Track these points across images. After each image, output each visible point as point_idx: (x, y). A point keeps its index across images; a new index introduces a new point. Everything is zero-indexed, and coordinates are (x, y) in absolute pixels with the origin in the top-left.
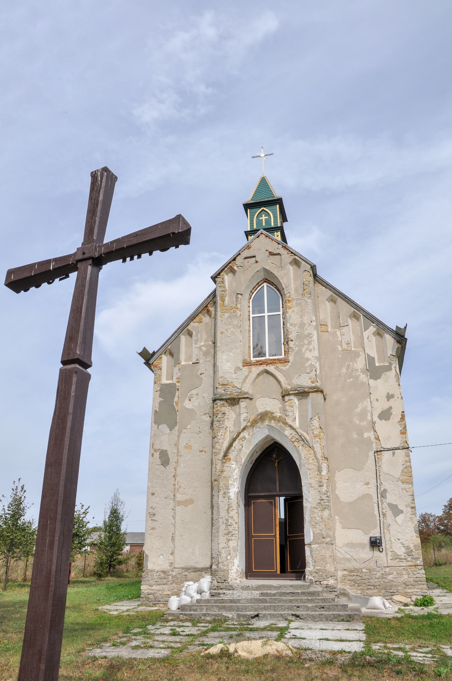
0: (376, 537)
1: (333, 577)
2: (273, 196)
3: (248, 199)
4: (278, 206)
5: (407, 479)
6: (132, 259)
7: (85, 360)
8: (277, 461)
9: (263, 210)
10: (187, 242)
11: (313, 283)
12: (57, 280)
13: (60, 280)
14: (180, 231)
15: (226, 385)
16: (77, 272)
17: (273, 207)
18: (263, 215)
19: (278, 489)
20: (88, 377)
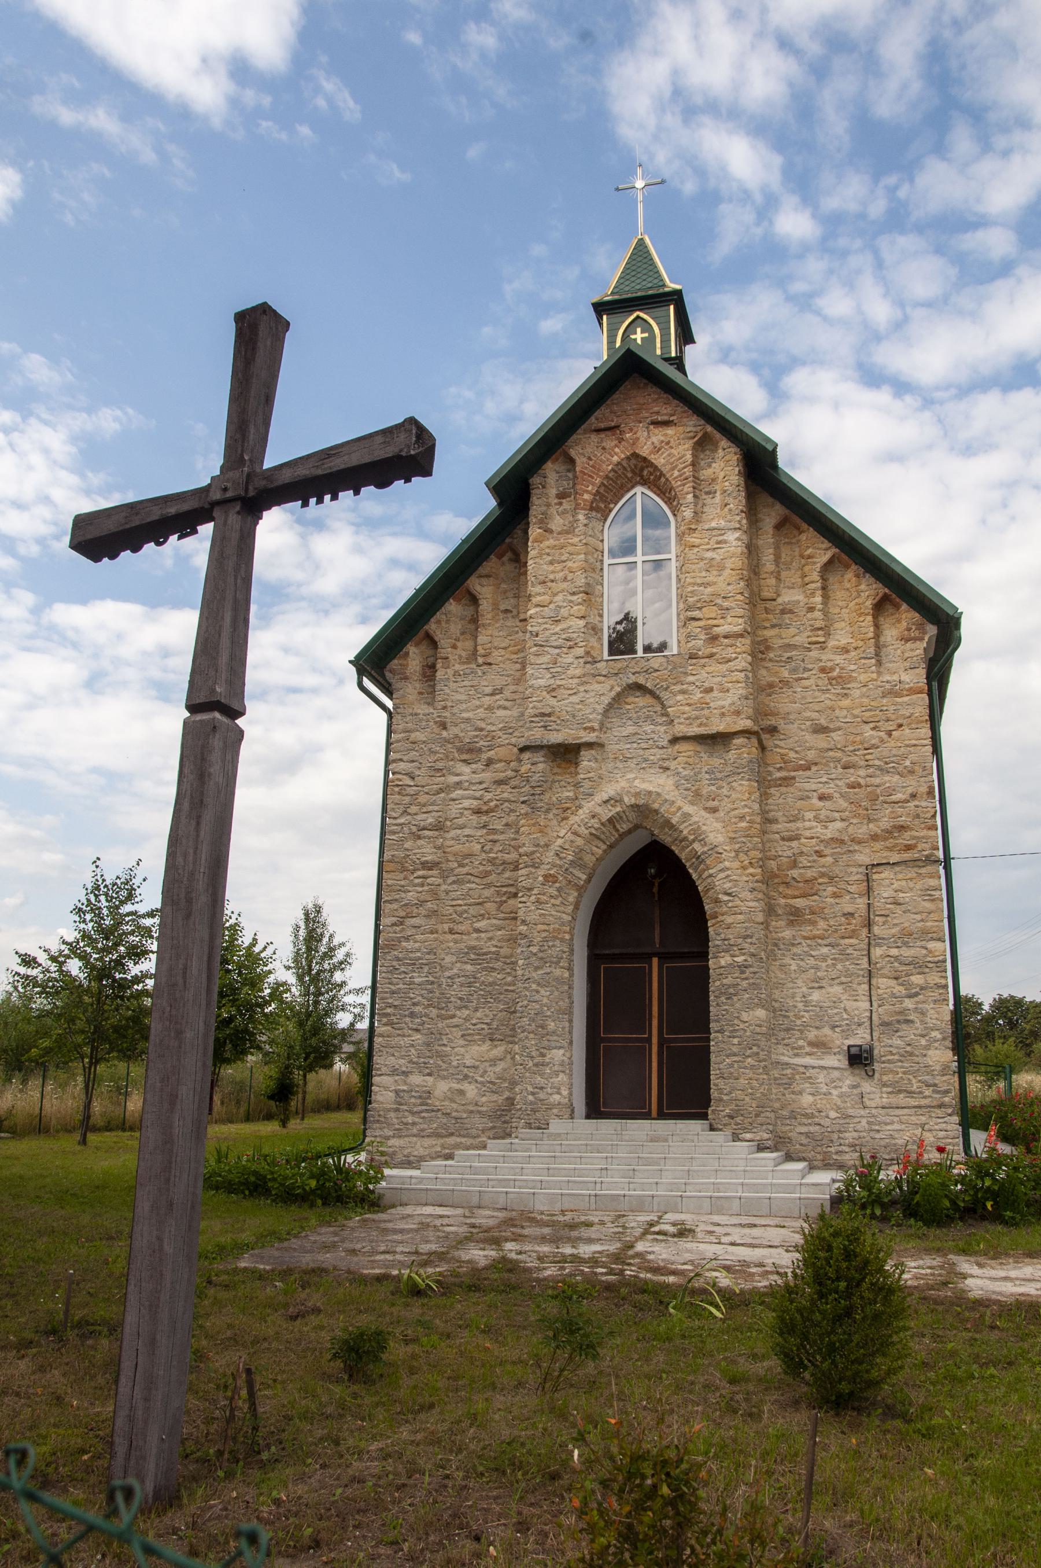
0: (860, 1046)
1: (764, 1127)
2: (661, 284)
3: (606, 292)
4: (672, 307)
5: (932, 927)
6: (320, 501)
7: (236, 706)
8: (657, 882)
9: (638, 317)
10: (427, 472)
11: (737, 502)
12: (173, 538)
13: (179, 538)
14: (412, 452)
15: (549, 715)
16: (213, 523)
17: (659, 312)
18: (639, 330)
19: (657, 940)
20: (241, 733)
